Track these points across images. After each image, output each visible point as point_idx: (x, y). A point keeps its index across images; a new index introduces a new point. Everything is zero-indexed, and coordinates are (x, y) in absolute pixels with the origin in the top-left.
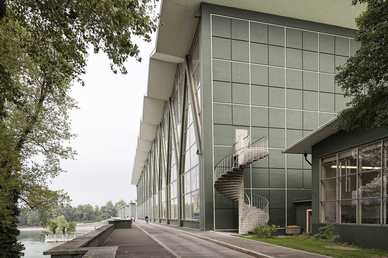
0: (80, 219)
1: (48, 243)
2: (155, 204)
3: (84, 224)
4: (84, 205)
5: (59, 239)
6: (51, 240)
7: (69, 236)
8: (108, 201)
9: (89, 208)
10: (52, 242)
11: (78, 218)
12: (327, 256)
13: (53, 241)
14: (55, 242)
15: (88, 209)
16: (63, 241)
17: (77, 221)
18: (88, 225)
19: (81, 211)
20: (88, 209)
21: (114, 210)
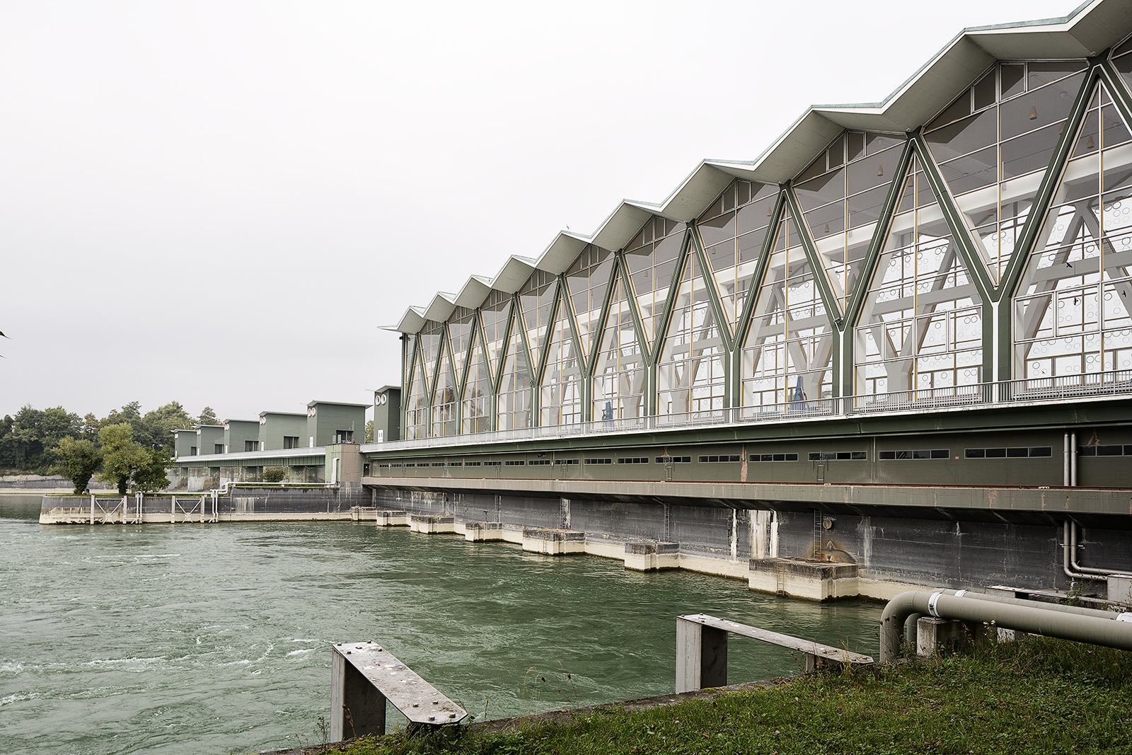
0: (26, 460)
1: (55, 526)
2: (754, 313)
3: (44, 477)
4: (44, 411)
5: (109, 514)
6: (73, 515)
7: (147, 502)
8: (433, 295)
9: (66, 421)
10: (74, 523)
11: (20, 456)
12: (796, 559)
13: (77, 521)
14: (92, 522)
15: (63, 424)
16: (92, 522)
17: (14, 466)
18: (59, 482)
19: (34, 431)
20: (63, 424)
21: (157, 434)
